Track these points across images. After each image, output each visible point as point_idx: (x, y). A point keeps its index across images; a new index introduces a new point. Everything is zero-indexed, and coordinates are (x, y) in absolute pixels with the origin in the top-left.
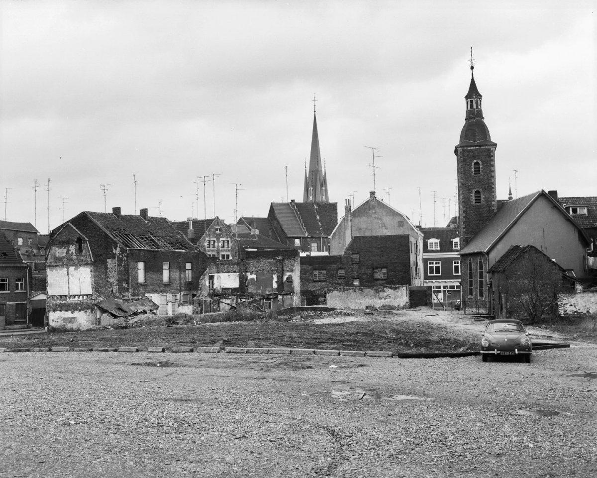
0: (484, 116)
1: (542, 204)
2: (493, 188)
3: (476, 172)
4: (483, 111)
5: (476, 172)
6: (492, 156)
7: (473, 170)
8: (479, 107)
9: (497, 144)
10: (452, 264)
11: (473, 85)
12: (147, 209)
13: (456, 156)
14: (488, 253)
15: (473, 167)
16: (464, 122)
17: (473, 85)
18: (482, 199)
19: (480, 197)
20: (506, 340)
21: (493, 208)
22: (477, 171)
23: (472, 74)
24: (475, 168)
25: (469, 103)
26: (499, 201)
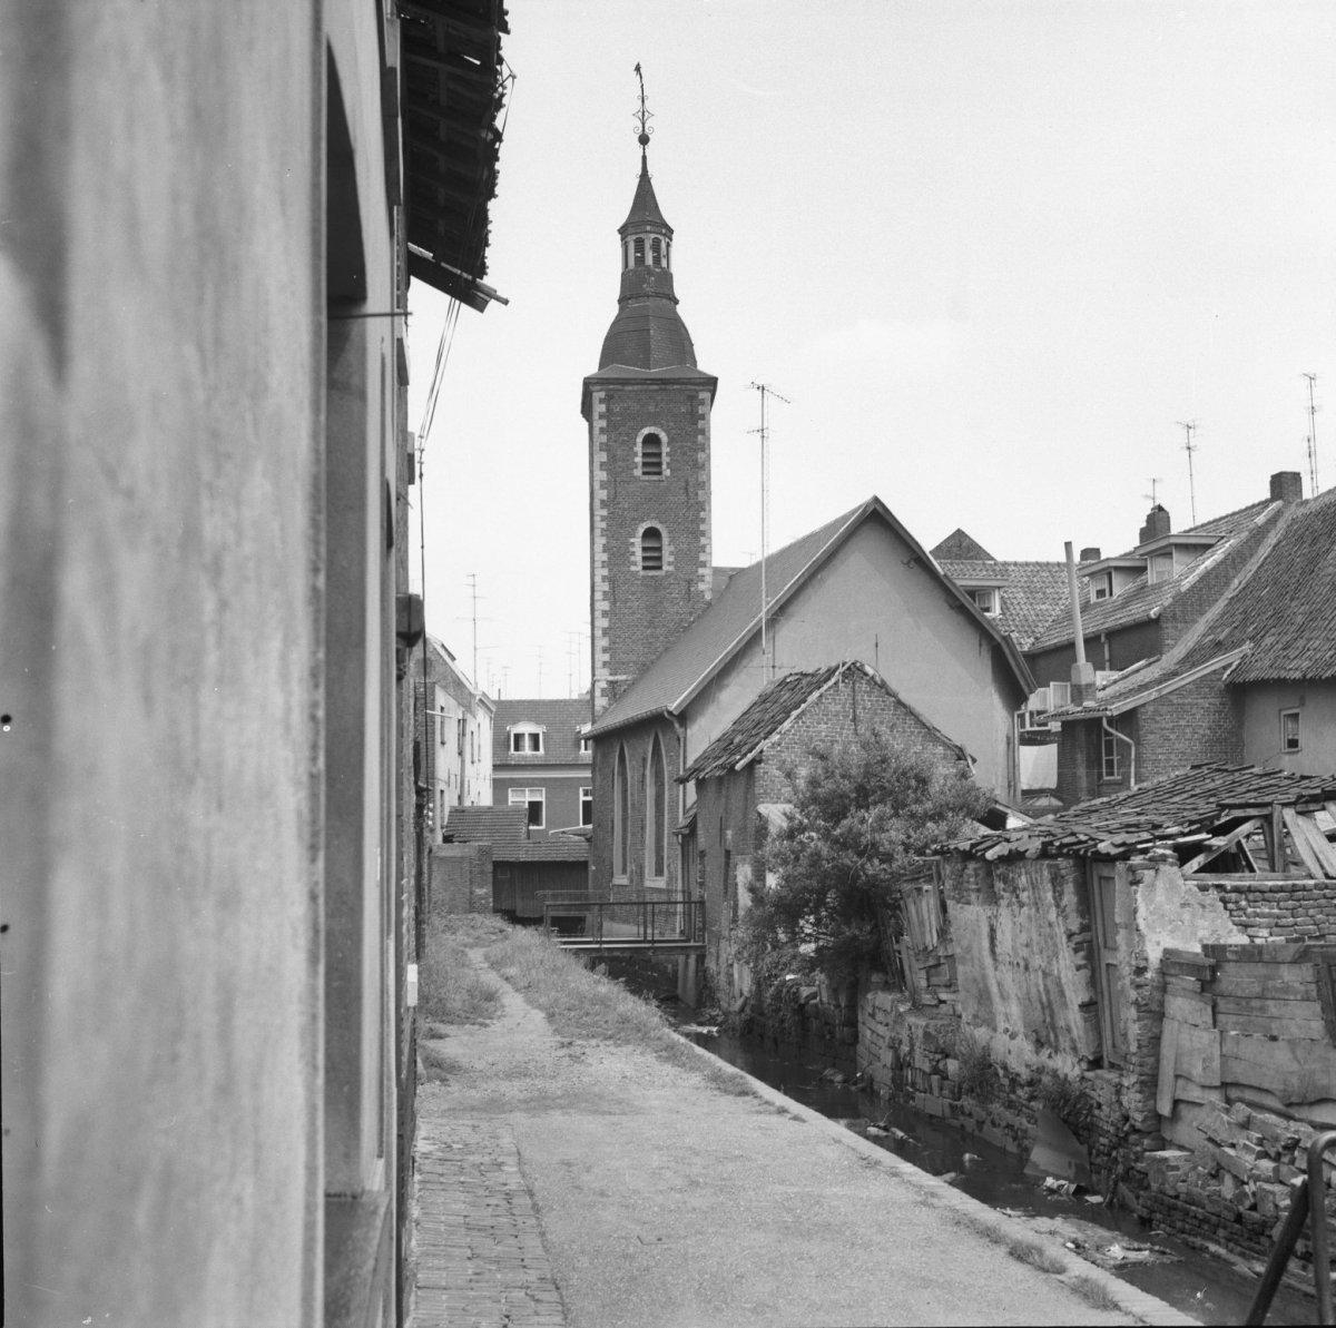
0: (678, 292)
1: (865, 568)
2: (703, 534)
3: (648, 564)
4: (675, 279)
5: (648, 564)
6: (703, 521)
7: (639, 459)
8: (664, 264)
9: (716, 379)
10: (578, 799)
11: (645, 195)
12: (876, 500)
13: (587, 424)
14: (684, 717)
15: (639, 448)
16: (613, 310)
17: (645, 195)
18: (667, 557)
19: (659, 549)
20: (54, 648)
21: (701, 586)
22: (652, 465)
23: (644, 158)
24: (644, 455)
25: (632, 246)
26: (717, 571)
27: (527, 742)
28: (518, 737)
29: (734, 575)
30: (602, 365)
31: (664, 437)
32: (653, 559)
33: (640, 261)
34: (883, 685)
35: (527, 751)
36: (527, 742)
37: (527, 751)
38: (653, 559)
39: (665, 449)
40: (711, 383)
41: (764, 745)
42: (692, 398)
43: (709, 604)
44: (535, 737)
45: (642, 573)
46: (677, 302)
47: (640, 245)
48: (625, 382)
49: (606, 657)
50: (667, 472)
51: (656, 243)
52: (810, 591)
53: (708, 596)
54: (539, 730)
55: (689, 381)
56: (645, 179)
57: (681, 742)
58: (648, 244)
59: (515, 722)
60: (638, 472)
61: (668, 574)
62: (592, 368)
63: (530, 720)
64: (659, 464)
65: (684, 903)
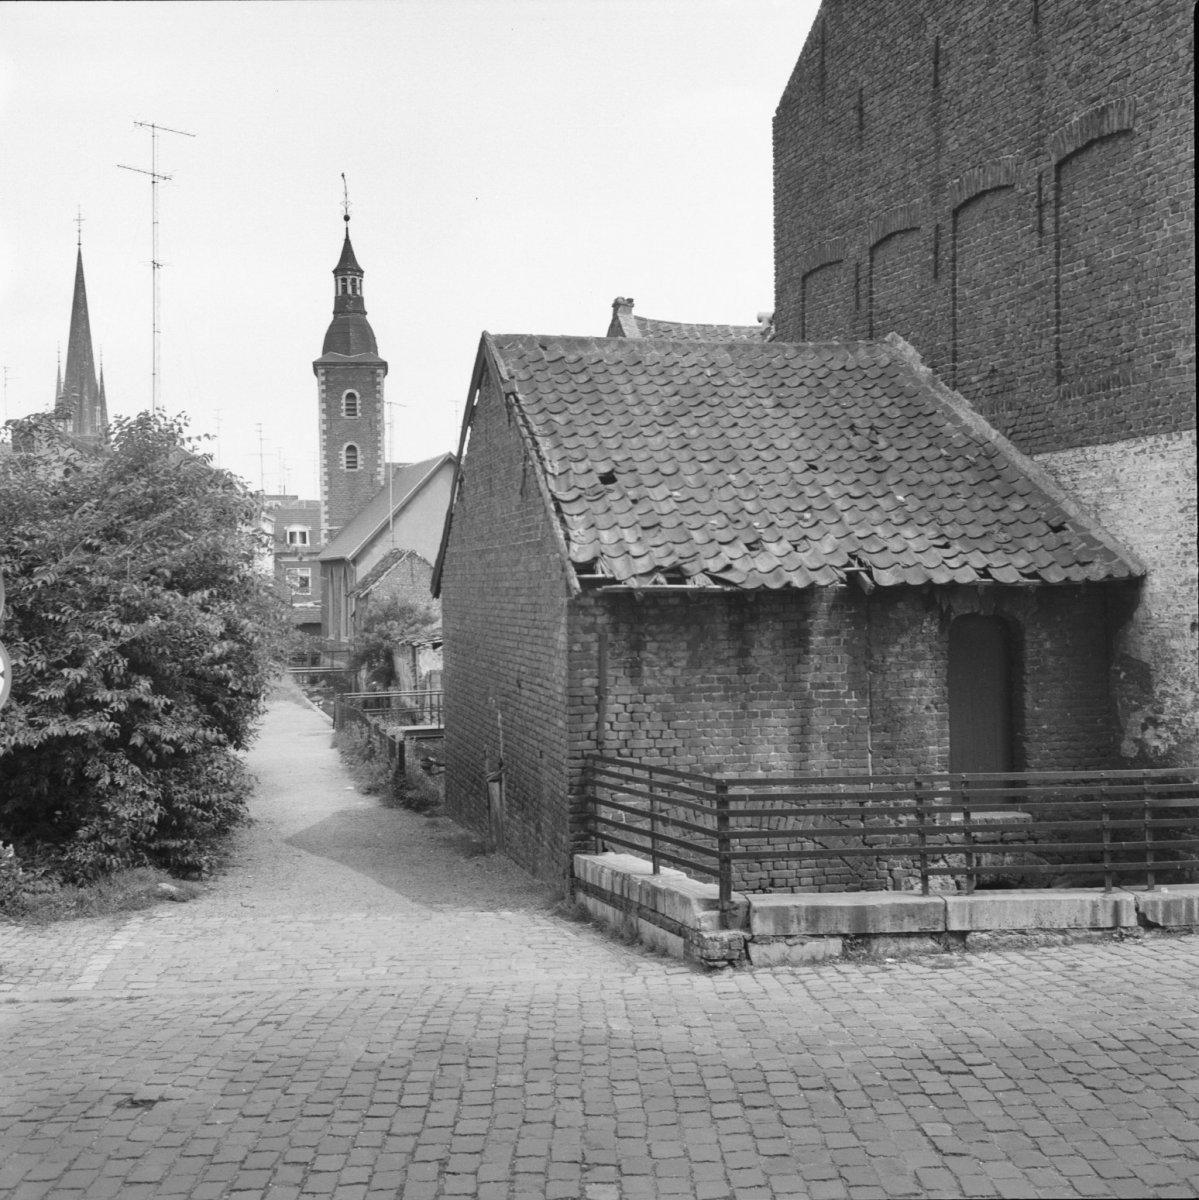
7: (344, 407)
14: (355, 561)
15: (344, 401)
16: (330, 318)
18: (360, 462)
19: (355, 457)
21: (379, 478)
22: (351, 410)
24: (347, 405)
26: (387, 466)
27: (298, 538)
28: (292, 535)
29: (399, 470)
30: (325, 351)
31: (357, 395)
32: (352, 463)
33: (345, 288)
34: (424, 561)
35: (298, 543)
36: (298, 538)
37: (298, 543)
38: (352, 463)
39: (358, 402)
40: (384, 365)
41: (372, 587)
42: (373, 373)
43: (383, 488)
44: (303, 535)
45: (346, 470)
46: (365, 313)
47: (344, 280)
48: (335, 364)
49: (327, 517)
50: (360, 415)
51: (354, 280)
52: (418, 498)
53: (382, 483)
54: (306, 529)
55: (371, 364)
56: (347, 242)
57: (353, 572)
58: (349, 281)
59: (290, 523)
60: (343, 414)
61: (360, 471)
62: (318, 355)
63: (299, 523)
64: (355, 410)
65: (333, 658)
